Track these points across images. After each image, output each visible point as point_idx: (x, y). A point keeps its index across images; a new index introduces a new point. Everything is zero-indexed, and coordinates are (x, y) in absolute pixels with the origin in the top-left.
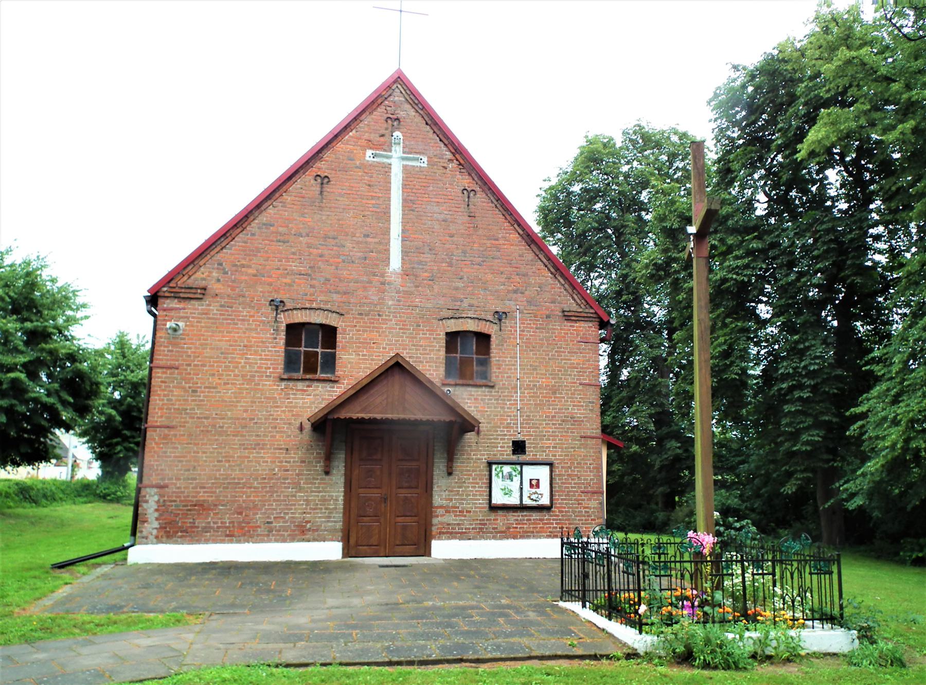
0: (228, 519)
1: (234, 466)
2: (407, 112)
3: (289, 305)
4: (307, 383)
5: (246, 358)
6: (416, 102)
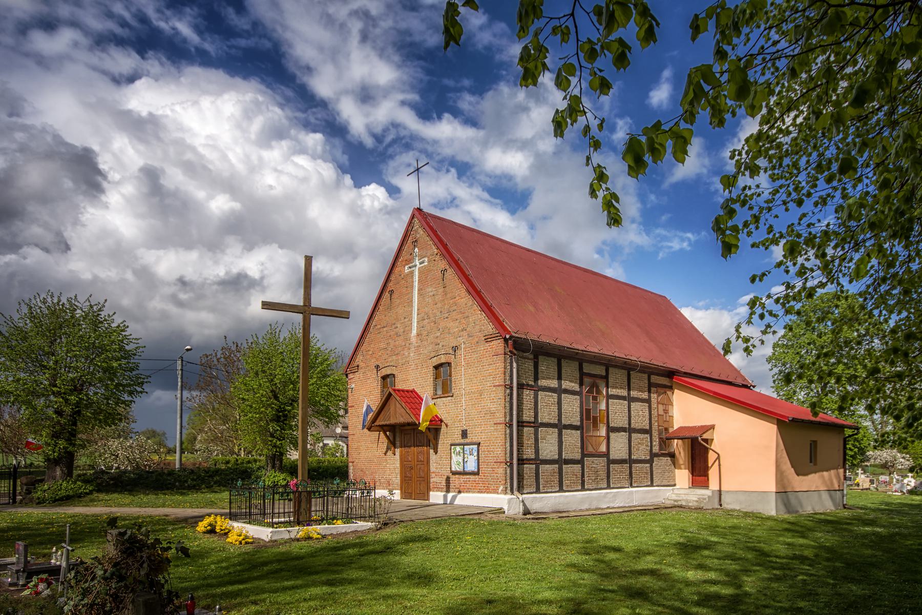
3: (381, 366)
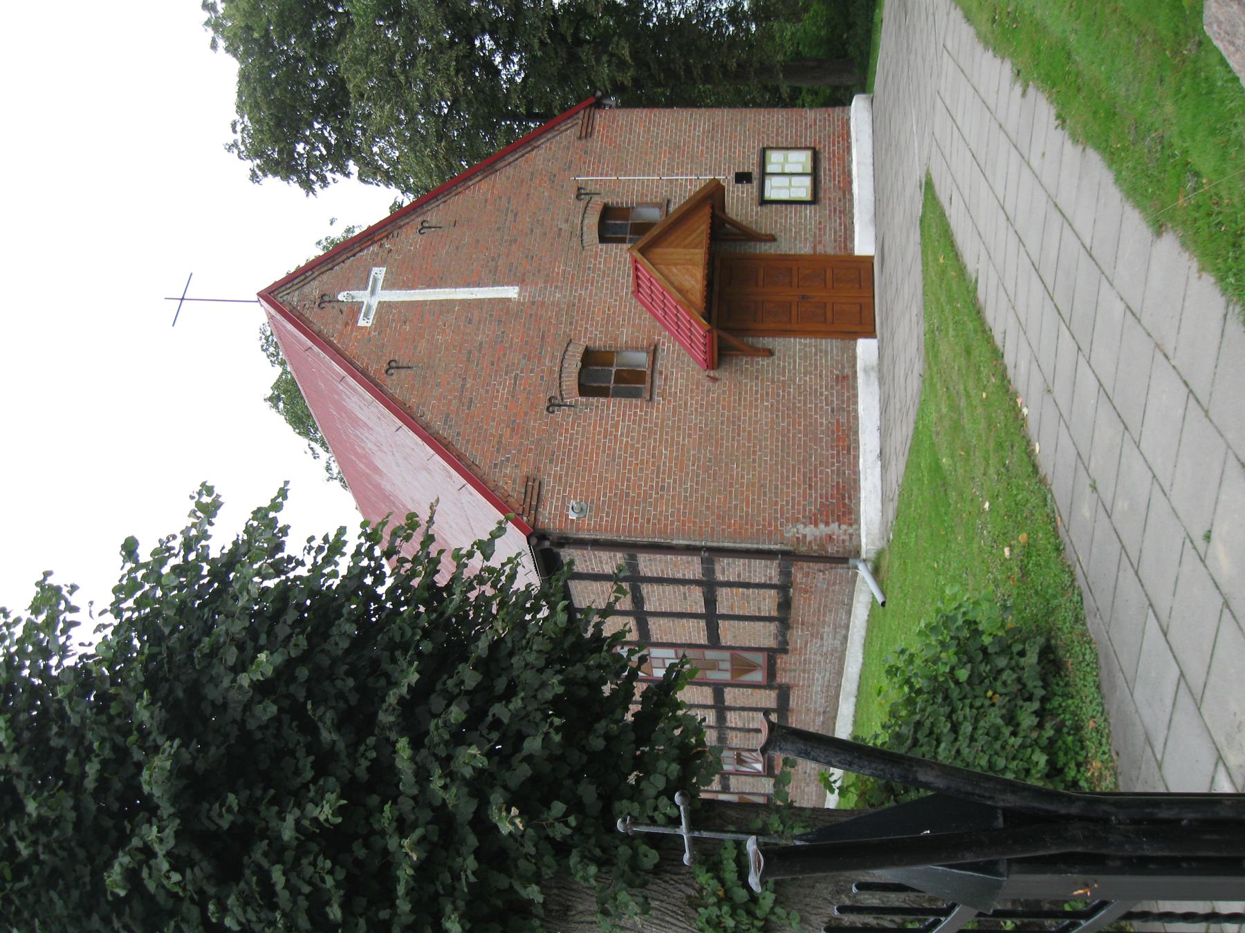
0: (827, 451)
1: (761, 446)
2: (313, 289)
3: (554, 392)
4: (657, 375)
5: (622, 435)
6: (303, 277)
